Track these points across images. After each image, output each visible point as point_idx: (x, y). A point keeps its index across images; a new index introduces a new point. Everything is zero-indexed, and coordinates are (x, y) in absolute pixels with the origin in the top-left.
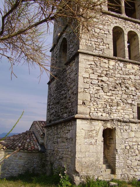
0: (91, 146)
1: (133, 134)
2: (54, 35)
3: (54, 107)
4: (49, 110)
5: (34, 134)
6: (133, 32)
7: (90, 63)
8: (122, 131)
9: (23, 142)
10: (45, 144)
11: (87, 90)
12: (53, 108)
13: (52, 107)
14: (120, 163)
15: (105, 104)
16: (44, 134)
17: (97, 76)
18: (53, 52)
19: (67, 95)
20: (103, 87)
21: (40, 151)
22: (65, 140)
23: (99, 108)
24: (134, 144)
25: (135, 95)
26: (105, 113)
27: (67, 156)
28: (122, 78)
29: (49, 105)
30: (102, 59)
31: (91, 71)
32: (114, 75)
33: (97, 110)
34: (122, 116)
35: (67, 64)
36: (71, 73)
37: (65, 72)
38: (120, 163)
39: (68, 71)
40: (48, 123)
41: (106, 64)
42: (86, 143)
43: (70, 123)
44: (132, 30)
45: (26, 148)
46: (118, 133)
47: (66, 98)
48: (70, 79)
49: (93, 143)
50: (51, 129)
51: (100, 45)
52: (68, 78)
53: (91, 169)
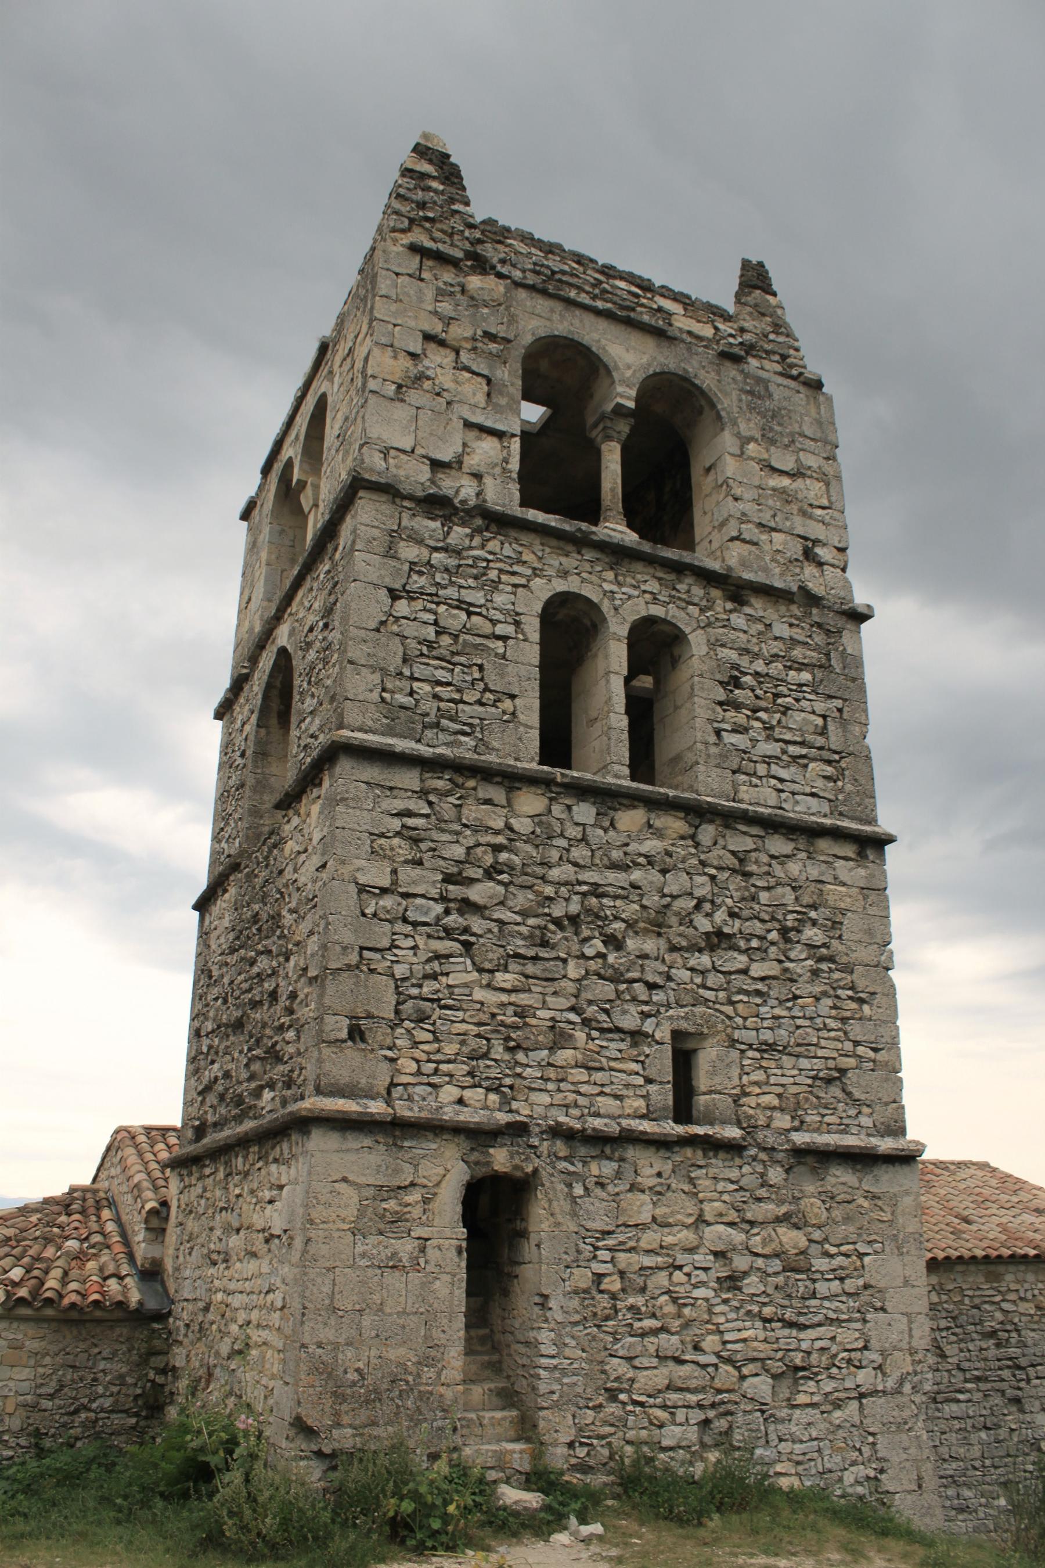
0: (394, 1279)
1: (642, 1207)
2: (239, 619)
3: (222, 1047)
4: (196, 1062)
5: (111, 1204)
6: (664, 621)
7: (399, 805)
8: (578, 1190)
9: (37, 1259)
10: (169, 1265)
11: (377, 956)
12: (217, 1053)
13: (210, 1047)
14: (564, 1372)
15: (478, 1036)
16: (164, 1204)
17: (440, 877)
18: (233, 722)
19: (282, 983)
20: (473, 939)
21: (137, 1310)
22: (259, 1246)
23: (449, 1062)
24: (648, 1261)
25: (659, 981)
26: (480, 1086)
27: (265, 1334)
28: (585, 888)
29: (196, 1034)
30: (471, 783)
31: (402, 849)
32: (539, 870)
33: (436, 1070)
34: (582, 1101)
35: (289, 801)
36: (303, 857)
37: (275, 846)
38: (564, 1372)
39: (291, 847)
40: (190, 1142)
41: (498, 810)
42: (363, 1263)
43: (285, 1146)
44: (657, 611)
45: (48, 1294)
46: (555, 1204)
47: (274, 995)
48: (298, 889)
49: (405, 1262)
50: (198, 1179)
51: (462, 701)
52: (286, 886)
53: (388, 1409)
